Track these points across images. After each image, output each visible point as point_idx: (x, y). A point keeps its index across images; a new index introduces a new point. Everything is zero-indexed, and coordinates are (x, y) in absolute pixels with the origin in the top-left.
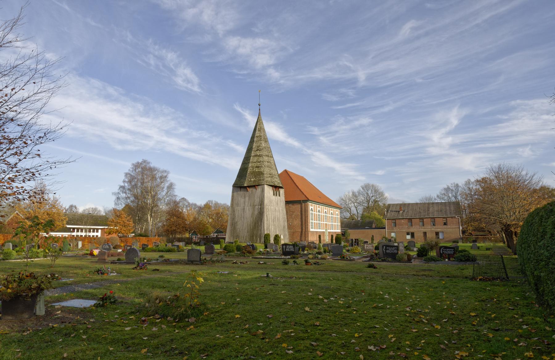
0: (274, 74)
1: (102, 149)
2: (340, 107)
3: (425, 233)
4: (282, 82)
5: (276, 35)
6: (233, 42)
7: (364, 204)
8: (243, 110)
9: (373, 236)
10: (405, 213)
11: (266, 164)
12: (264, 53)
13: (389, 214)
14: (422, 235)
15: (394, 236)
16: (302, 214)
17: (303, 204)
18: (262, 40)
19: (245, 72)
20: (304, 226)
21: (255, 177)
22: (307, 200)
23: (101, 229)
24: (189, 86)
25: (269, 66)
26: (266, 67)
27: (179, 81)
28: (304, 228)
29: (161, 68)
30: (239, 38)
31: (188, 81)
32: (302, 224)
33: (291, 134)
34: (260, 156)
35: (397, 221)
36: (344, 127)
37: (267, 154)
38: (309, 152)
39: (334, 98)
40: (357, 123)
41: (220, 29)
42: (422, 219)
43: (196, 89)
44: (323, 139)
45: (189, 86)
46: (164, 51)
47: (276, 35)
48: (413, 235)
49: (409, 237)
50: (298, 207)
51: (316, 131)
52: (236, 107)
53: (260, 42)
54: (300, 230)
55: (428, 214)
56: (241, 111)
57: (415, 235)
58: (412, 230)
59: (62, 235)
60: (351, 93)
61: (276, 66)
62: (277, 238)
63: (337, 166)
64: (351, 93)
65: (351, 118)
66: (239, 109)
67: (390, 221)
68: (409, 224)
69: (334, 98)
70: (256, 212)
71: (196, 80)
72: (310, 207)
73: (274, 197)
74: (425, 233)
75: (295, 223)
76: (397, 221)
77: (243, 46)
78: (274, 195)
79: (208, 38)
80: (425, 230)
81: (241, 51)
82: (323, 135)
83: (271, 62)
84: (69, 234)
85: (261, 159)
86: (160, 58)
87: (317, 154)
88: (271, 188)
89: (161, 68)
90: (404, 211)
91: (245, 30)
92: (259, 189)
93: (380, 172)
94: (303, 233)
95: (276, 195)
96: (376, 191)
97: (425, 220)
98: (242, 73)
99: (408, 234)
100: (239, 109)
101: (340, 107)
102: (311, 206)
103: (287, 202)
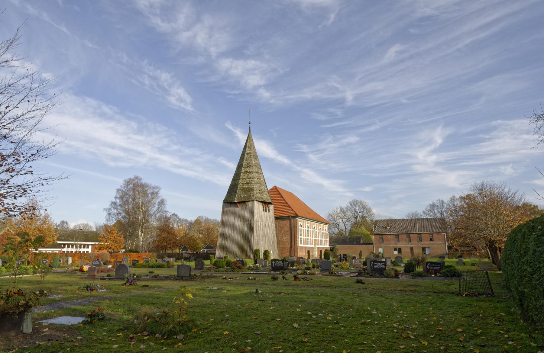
0: (266, 94)
1: (99, 164)
2: (328, 126)
3: (412, 249)
4: (272, 101)
5: (267, 57)
6: (225, 63)
7: (352, 220)
8: (234, 129)
9: (361, 251)
10: (392, 229)
11: (256, 180)
12: (255, 74)
13: (376, 230)
14: (409, 250)
15: (382, 252)
16: (291, 230)
17: (292, 220)
18: (253, 62)
19: (237, 92)
20: (293, 241)
21: (245, 193)
22: (296, 216)
23: (92, 245)
24: (182, 105)
25: (260, 86)
26: (256, 88)
27: (173, 100)
28: (293, 244)
29: (155, 87)
30: (231, 59)
31: (181, 100)
32: (291, 240)
33: (281, 151)
34: (250, 172)
35: (385, 237)
36: (332, 145)
37: (257, 170)
38: (299, 168)
39: (322, 117)
40: (345, 141)
41: (213, 51)
42: (409, 235)
43: (189, 108)
44: (313, 157)
45: (182, 105)
46: (159, 72)
47: (267, 57)
48: (400, 250)
49: (396, 253)
50: (288, 222)
51: (305, 148)
52: (227, 125)
53: (251, 63)
54: (289, 246)
55: (415, 230)
56: (233, 129)
57: (402, 250)
58: (399, 246)
59: (53, 251)
60: (339, 112)
61: (267, 87)
62: (266, 253)
63: (326, 183)
64: (339, 112)
65: (339, 136)
66: (230, 127)
67: (378, 237)
68: (396, 239)
69: (322, 117)
70: (246, 228)
71: (189, 99)
72: (299, 223)
73: (264, 213)
74: (412, 249)
75: (284, 239)
76: (385, 237)
77: (234, 67)
78: (263, 210)
79: (201, 60)
80: (411, 246)
81: (234, 72)
82: (312, 152)
83: (262, 82)
84: (60, 250)
85: (251, 176)
86: (154, 78)
87: (306, 171)
88: (261, 204)
89: (155, 87)
90: (391, 227)
91: (236, 53)
92: (249, 205)
93: (367, 189)
94: (293, 248)
95: (266, 211)
96: (364, 207)
97: (411, 236)
98: (233, 92)
99: (395, 249)
100: (230, 127)
101: (328, 126)
102: (300, 222)
103: (277, 218)
